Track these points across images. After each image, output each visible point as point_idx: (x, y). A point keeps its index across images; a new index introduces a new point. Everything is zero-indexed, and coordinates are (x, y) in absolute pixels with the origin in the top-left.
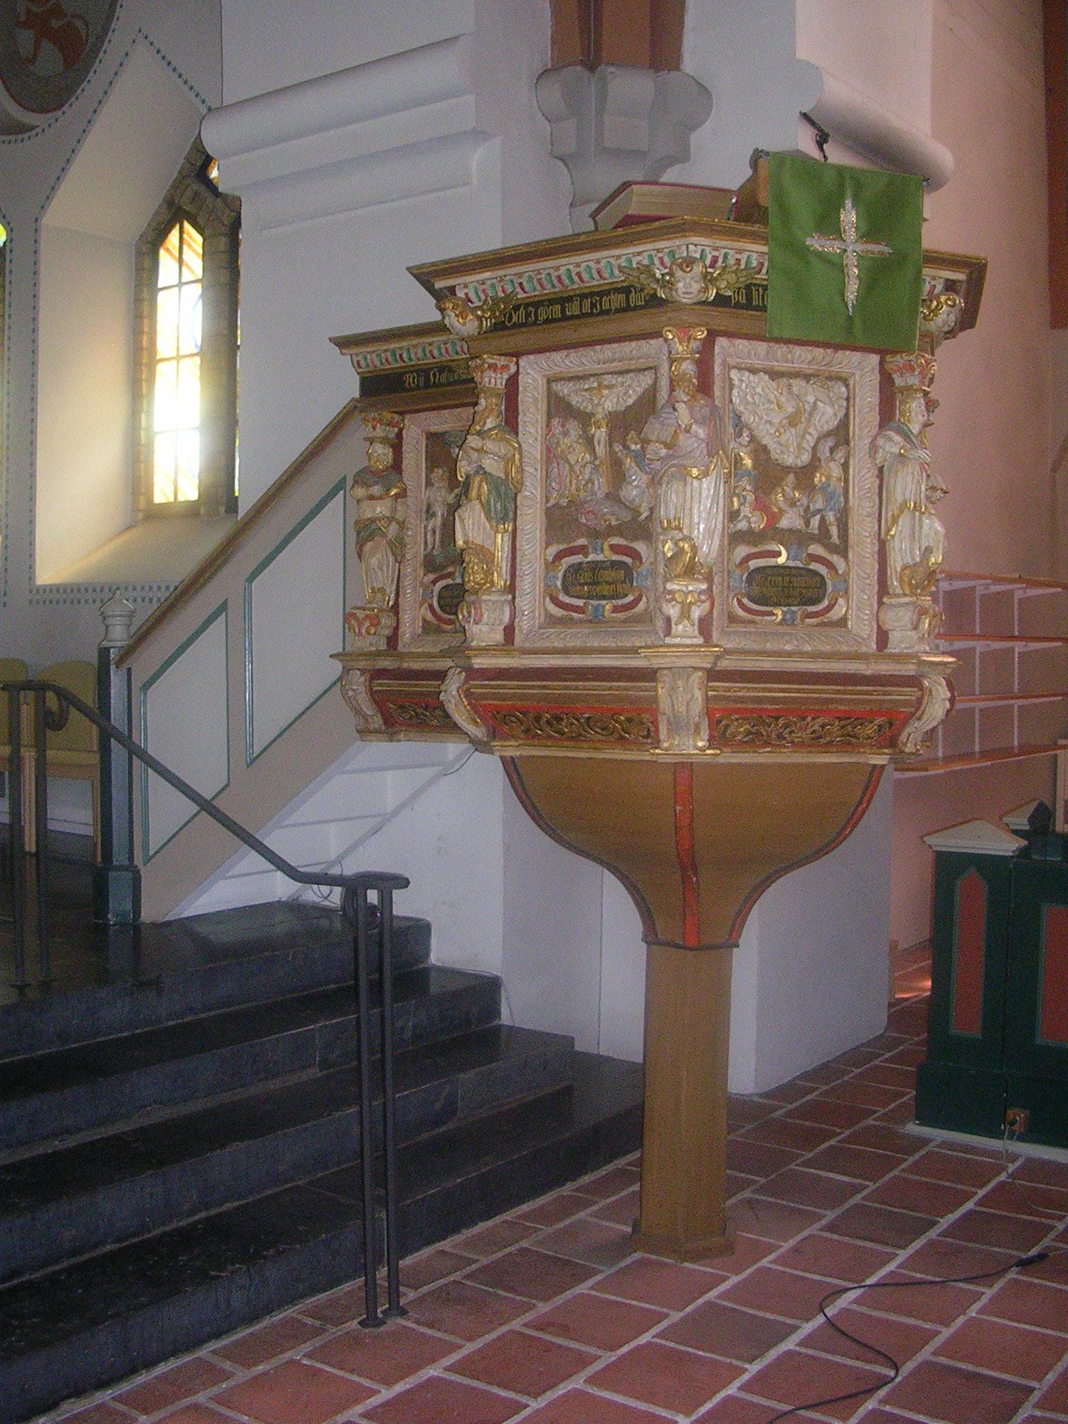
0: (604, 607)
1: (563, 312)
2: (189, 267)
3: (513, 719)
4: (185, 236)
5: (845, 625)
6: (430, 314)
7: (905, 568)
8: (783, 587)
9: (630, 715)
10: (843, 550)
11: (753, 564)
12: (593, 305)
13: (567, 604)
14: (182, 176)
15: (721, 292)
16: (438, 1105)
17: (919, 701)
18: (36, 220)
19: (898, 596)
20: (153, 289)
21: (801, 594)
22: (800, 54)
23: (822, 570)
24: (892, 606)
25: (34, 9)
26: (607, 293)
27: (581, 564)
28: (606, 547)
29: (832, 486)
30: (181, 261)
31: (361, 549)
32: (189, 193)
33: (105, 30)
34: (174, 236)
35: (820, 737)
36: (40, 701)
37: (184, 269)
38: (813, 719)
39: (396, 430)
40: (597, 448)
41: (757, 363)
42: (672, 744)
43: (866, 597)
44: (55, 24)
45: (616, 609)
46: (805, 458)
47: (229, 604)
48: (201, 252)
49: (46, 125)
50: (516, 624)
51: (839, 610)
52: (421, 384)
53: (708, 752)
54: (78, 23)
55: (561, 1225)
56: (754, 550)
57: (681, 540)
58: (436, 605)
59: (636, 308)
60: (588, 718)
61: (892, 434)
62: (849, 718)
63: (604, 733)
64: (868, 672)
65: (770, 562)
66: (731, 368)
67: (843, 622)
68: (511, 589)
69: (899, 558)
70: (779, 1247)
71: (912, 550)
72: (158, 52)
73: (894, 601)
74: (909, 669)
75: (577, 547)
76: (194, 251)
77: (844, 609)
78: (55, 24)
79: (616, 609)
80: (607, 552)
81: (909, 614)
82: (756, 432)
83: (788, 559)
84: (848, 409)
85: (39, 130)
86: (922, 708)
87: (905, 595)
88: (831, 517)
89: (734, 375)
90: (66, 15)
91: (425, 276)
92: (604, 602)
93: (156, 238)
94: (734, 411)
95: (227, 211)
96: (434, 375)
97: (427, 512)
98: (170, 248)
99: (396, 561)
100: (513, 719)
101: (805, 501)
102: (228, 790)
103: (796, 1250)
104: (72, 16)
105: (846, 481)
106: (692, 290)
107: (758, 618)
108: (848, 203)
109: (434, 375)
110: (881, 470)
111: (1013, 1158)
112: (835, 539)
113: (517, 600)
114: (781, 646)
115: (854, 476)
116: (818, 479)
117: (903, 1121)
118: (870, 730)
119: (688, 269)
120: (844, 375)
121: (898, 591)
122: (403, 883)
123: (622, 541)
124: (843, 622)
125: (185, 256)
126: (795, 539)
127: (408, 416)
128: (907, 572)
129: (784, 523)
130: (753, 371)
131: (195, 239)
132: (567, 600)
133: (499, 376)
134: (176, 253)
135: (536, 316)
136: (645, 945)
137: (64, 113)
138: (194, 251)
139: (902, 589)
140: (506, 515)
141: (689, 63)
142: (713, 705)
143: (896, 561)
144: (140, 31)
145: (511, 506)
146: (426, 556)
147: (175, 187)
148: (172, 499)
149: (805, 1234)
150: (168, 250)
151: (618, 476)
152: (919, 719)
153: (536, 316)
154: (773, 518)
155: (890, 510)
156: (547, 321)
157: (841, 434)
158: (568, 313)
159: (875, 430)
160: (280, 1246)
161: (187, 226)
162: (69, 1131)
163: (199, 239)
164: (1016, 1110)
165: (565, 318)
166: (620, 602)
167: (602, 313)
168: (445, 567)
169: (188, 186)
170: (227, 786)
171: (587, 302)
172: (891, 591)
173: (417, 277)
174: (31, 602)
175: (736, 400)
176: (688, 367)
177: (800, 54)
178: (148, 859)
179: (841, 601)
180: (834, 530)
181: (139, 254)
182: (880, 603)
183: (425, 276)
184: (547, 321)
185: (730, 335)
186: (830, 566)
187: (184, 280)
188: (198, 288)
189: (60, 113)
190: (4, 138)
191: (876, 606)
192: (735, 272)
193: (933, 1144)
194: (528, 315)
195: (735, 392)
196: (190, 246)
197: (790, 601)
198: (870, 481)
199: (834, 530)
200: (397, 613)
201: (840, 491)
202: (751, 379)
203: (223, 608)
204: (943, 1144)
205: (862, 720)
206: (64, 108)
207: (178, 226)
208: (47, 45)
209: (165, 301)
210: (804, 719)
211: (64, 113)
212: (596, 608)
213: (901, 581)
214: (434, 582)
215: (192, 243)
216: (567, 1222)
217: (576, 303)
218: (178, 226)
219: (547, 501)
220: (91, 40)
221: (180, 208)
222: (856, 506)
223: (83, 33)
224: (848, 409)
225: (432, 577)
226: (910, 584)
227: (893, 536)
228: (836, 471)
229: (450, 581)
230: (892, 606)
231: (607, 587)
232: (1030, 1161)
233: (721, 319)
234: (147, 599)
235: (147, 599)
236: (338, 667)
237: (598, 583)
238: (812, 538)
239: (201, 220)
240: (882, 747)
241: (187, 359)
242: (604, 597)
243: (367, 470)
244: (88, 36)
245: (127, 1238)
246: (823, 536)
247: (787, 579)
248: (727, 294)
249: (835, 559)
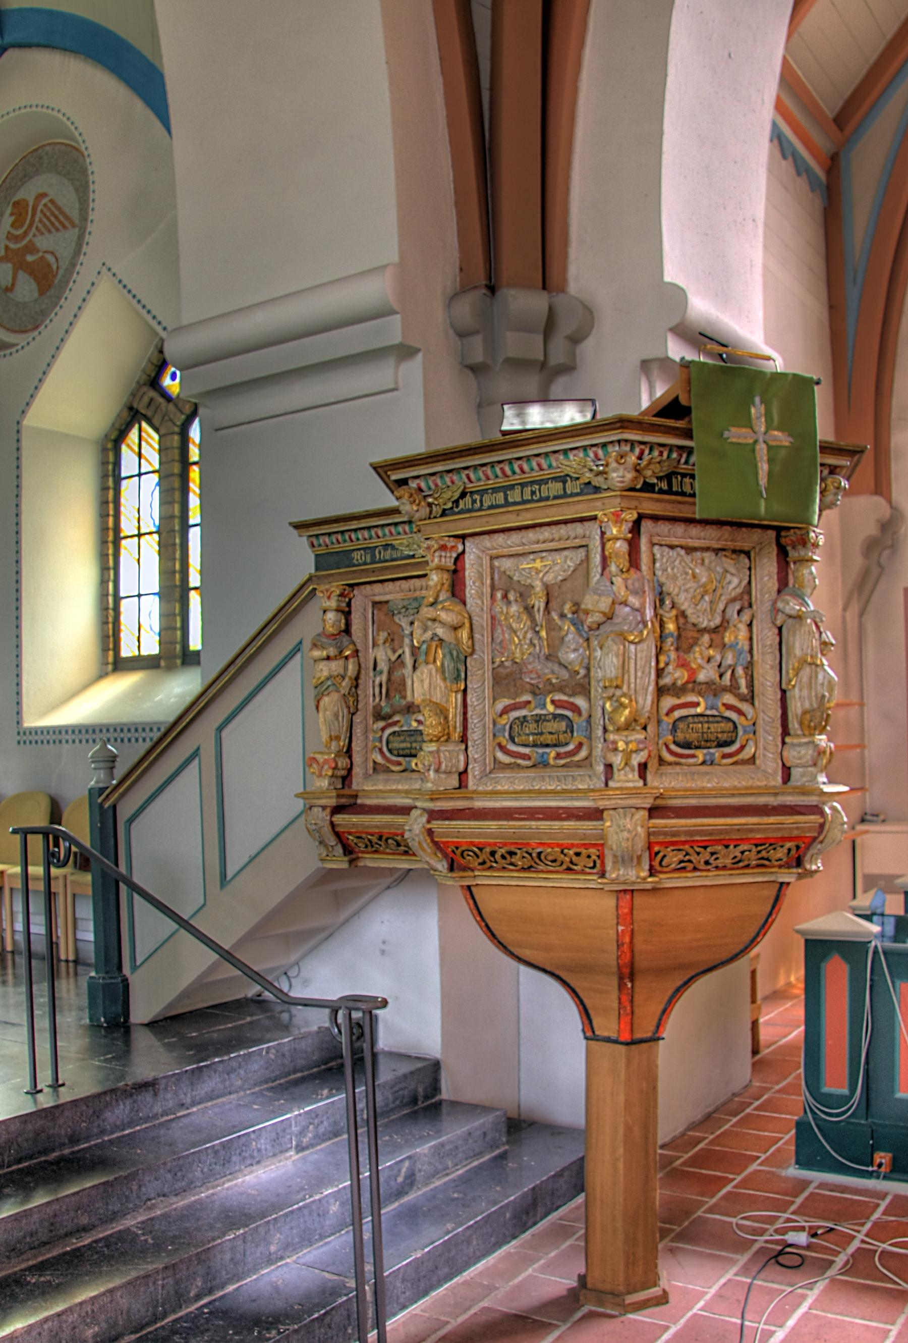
0: (548, 754)
1: (506, 498)
2: (147, 460)
3: (471, 853)
4: (143, 434)
5: (754, 763)
6: (389, 501)
7: (805, 713)
8: (703, 733)
9: (578, 850)
10: (751, 699)
11: (677, 714)
12: (533, 493)
13: (515, 752)
14: (140, 385)
15: (647, 480)
16: (400, 1179)
17: (822, 826)
18: (18, 423)
19: (798, 736)
20: (118, 480)
21: (717, 738)
22: (667, 279)
23: (733, 716)
24: (793, 745)
25: (12, 246)
26: (546, 482)
27: (525, 717)
28: (548, 700)
29: (740, 644)
30: (140, 455)
31: (318, 702)
32: (146, 400)
33: (73, 265)
34: (134, 435)
35: (740, 861)
36: (59, 860)
37: (143, 461)
38: (735, 847)
39: (347, 600)
40: (537, 616)
41: (675, 542)
42: (618, 875)
43: (771, 738)
44: (30, 258)
45: (558, 756)
46: (718, 621)
47: (202, 751)
48: (157, 447)
49: (25, 343)
50: (469, 770)
51: (750, 751)
52: (368, 560)
53: (650, 880)
54: (50, 259)
55: (516, 1281)
56: (677, 701)
57: (622, 696)
58: (385, 749)
59: (572, 495)
60: (539, 854)
61: (789, 598)
62: (764, 844)
63: (554, 864)
64: (775, 804)
65: (692, 711)
66: (653, 545)
67: (752, 760)
68: (464, 739)
69: (799, 705)
70: (706, 1293)
71: (810, 698)
72: (120, 281)
73: (795, 741)
74: (813, 800)
75: (520, 703)
76: (151, 446)
77: (753, 750)
78: (30, 258)
79: (558, 756)
80: (551, 708)
81: (810, 752)
82: (676, 600)
83: (706, 708)
84: (750, 576)
85: (19, 347)
86: (825, 832)
87: (804, 735)
88: (740, 671)
89: (656, 549)
90: (38, 251)
91: (381, 470)
92: (547, 750)
93: (118, 437)
94: (658, 581)
95: (179, 414)
96: (380, 553)
97: (375, 669)
98: (131, 444)
99: (349, 712)
100: (471, 853)
101: (718, 658)
102: (205, 909)
103: (719, 1296)
104: (46, 252)
105: (751, 639)
106: (625, 479)
107: (683, 761)
108: (757, 400)
109: (380, 553)
110: (780, 629)
111: (883, 1196)
112: (744, 690)
113: (470, 749)
114: (704, 784)
115: (757, 636)
116: (728, 638)
117: (784, 1165)
118: (781, 853)
119: (623, 461)
120: (746, 549)
121: (799, 732)
122: (384, 1003)
123: (564, 698)
124: (752, 760)
125: (143, 451)
126: (712, 689)
127: (356, 588)
128: (808, 717)
129: (702, 677)
130: (672, 547)
131: (152, 437)
132: (512, 747)
133: (448, 555)
134: (137, 449)
135: (481, 501)
136: (584, 1042)
137: (40, 333)
138: (151, 446)
139: (802, 730)
140: (459, 675)
141: (573, 288)
142: (653, 839)
143: (796, 707)
144: (104, 264)
145: (462, 669)
146: (374, 707)
147: (133, 395)
148: (137, 653)
149: (723, 1281)
150: (128, 446)
151: (556, 643)
152: (821, 842)
153: (481, 501)
154: (693, 673)
155: (790, 665)
156: (491, 507)
157: (745, 599)
158: (510, 500)
159: (774, 594)
160: (280, 1327)
161: (144, 425)
162: (85, 1229)
163: (156, 437)
164: (882, 1154)
165: (507, 504)
166: (562, 750)
167: (541, 499)
168: (390, 717)
169: (144, 393)
170: (204, 905)
171: (528, 490)
172: (792, 732)
173: (375, 469)
174: (19, 743)
175: (659, 573)
176: (621, 546)
177: (667, 279)
178: (134, 967)
179: (751, 743)
180: (743, 682)
181: (104, 450)
182: (784, 743)
183: (381, 470)
184: (491, 507)
185: (655, 518)
186: (740, 713)
187: (143, 471)
188: (155, 478)
189: (36, 333)
190: (2, 353)
191: (780, 745)
192: (659, 463)
193: (813, 1185)
194: (474, 501)
195: (658, 565)
196: (148, 443)
197: (709, 744)
198: (771, 636)
199: (743, 682)
200: (350, 757)
201: (746, 648)
202: (671, 554)
203: (195, 754)
204: (822, 1185)
205: (773, 844)
206: (40, 329)
207: (137, 426)
208: (23, 277)
209: (127, 488)
210: (727, 847)
211: (40, 333)
212: (543, 755)
213: (801, 723)
214: (383, 729)
215: (149, 440)
216: (520, 1278)
217: (518, 490)
218: (137, 426)
219: (493, 663)
220: (61, 272)
221: (137, 412)
222: (760, 661)
223: (55, 267)
224: (750, 576)
225: (381, 724)
226: (809, 726)
227: (794, 686)
228: (743, 633)
229: (396, 729)
230: (793, 745)
231: (550, 737)
232: (897, 1197)
233: (650, 504)
234: (119, 740)
235: (119, 740)
236: (300, 804)
237: (542, 734)
238: (725, 689)
239: (156, 421)
240: (789, 867)
241: (147, 536)
242: (547, 746)
243: (323, 634)
244: (58, 268)
245: (142, 1328)
246: (733, 688)
247: (706, 726)
248: (651, 482)
249: (745, 707)
